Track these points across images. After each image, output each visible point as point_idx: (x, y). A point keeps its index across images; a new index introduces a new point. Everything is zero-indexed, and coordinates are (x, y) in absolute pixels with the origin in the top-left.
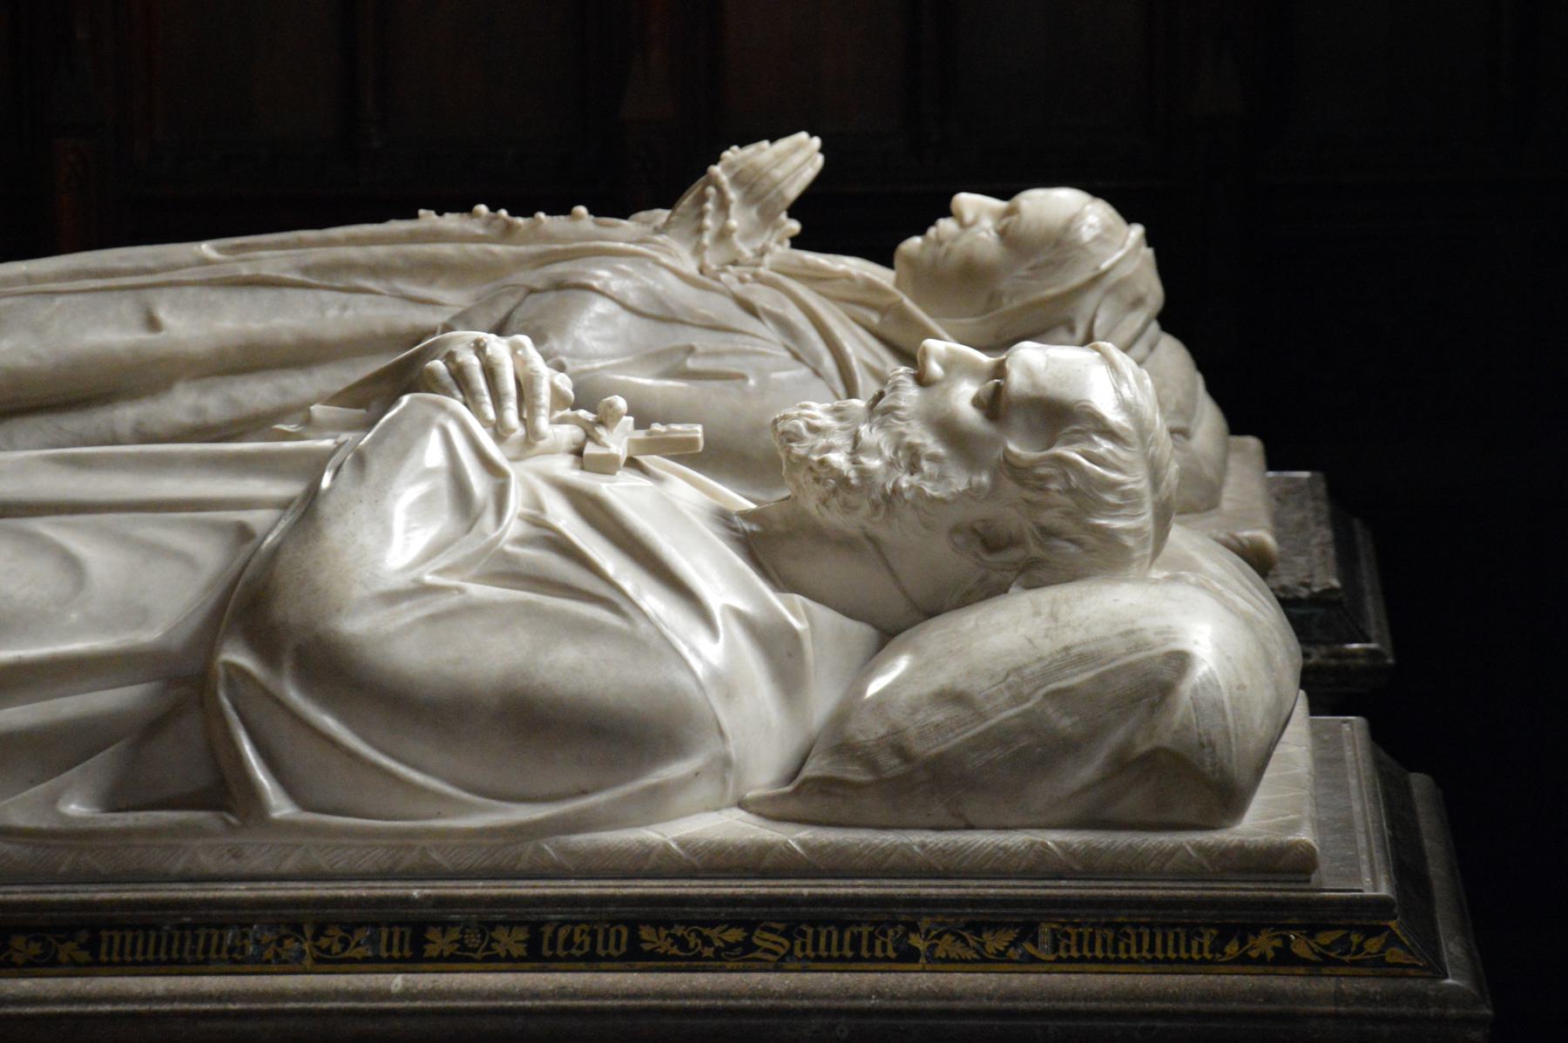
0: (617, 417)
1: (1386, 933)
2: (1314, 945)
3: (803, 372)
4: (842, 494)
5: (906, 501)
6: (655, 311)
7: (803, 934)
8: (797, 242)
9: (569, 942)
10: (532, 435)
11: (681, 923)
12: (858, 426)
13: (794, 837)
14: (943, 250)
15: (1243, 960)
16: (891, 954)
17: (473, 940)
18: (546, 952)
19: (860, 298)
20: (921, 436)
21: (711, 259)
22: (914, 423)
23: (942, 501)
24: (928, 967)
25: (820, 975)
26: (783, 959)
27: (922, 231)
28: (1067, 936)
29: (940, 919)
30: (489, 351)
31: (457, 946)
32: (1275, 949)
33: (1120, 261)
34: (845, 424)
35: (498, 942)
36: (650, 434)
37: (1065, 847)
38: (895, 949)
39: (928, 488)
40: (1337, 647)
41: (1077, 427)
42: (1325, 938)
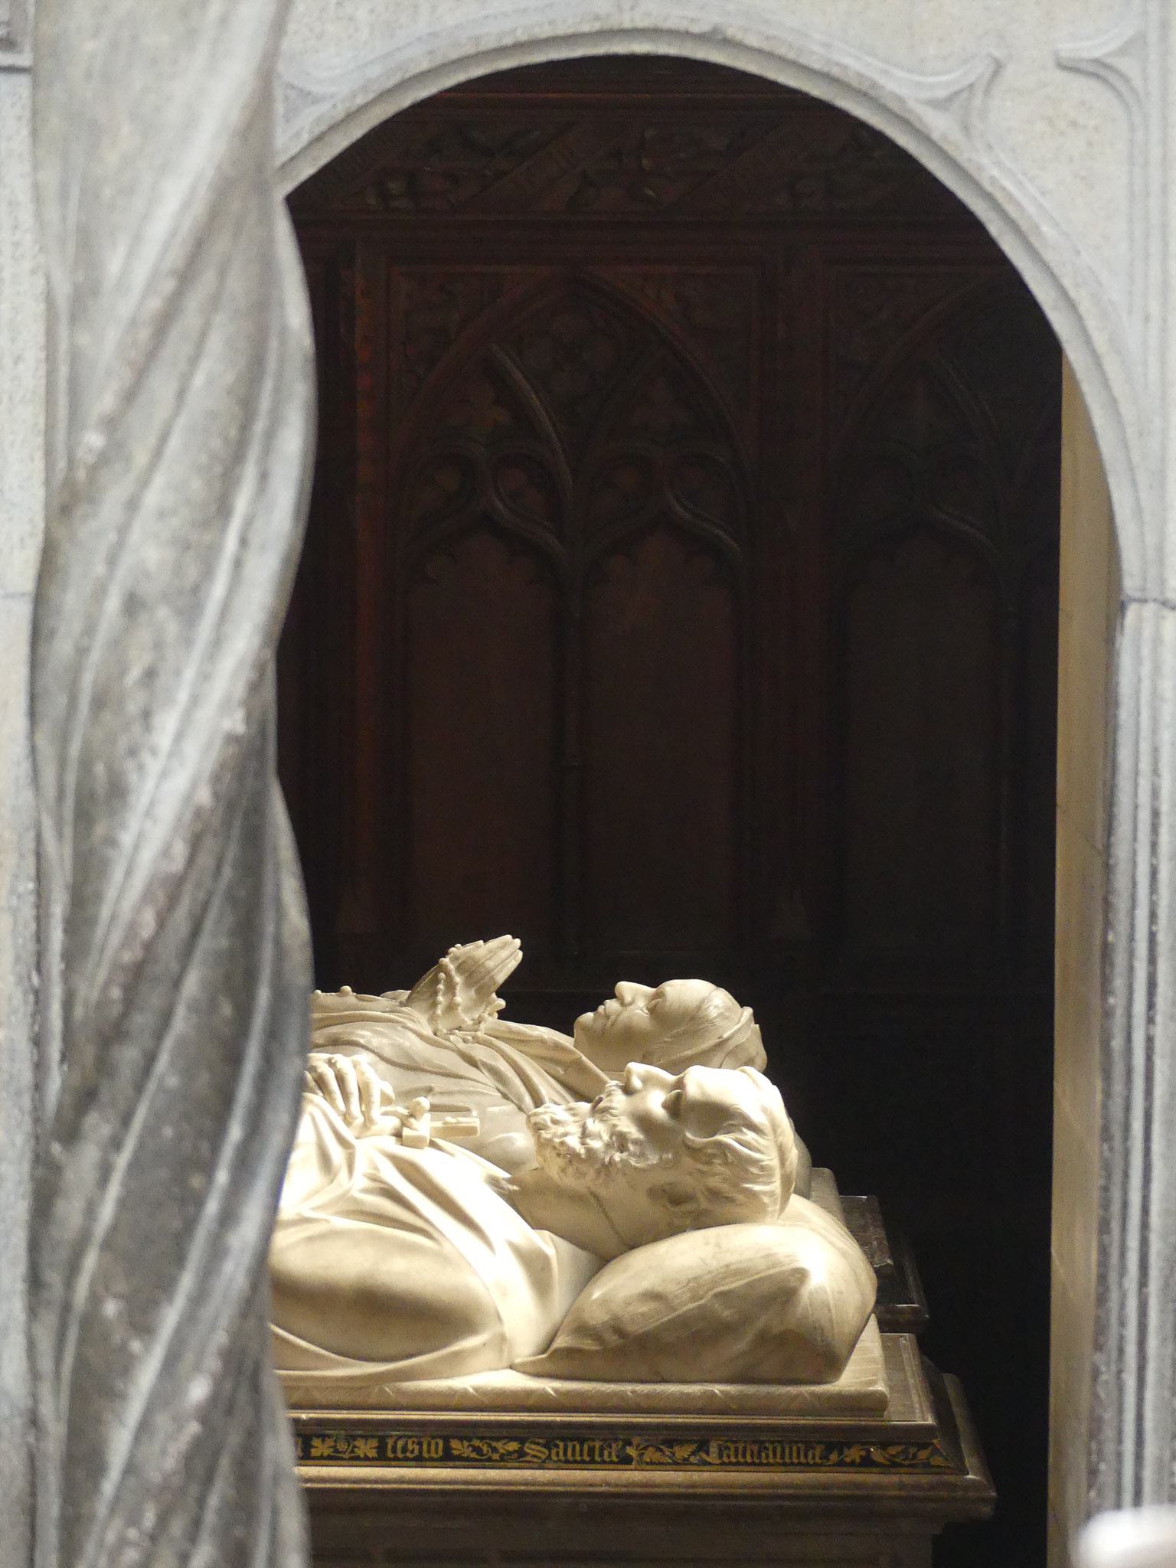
0: (423, 1112)
1: (930, 1448)
2: (887, 1456)
3: (510, 1107)
4: (576, 1164)
5: (618, 1170)
6: (404, 1062)
7: (557, 1446)
8: (503, 1015)
9: (405, 1449)
10: (368, 1122)
11: (478, 1438)
12: (586, 1119)
13: (549, 1386)
14: (609, 1023)
15: (840, 1464)
16: (615, 1459)
17: (342, 1446)
18: (390, 1455)
19: (550, 1059)
20: (627, 1126)
21: (443, 1027)
22: (623, 1118)
23: (643, 1170)
24: (639, 1467)
25: (568, 1472)
26: (544, 1462)
27: (594, 1009)
28: (728, 1448)
29: (647, 1437)
30: (339, 1066)
31: (332, 1450)
32: (861, 1457)
33: (736, 1032)
34: (576, 1119)
35: (359, 1448)
36: (445, 1123)
37: (725, 1394)
38: (617, 1456)
39: (633, 1162)
40: (891, 1306)
41: (731, 1122)
42: (893, 1450)
